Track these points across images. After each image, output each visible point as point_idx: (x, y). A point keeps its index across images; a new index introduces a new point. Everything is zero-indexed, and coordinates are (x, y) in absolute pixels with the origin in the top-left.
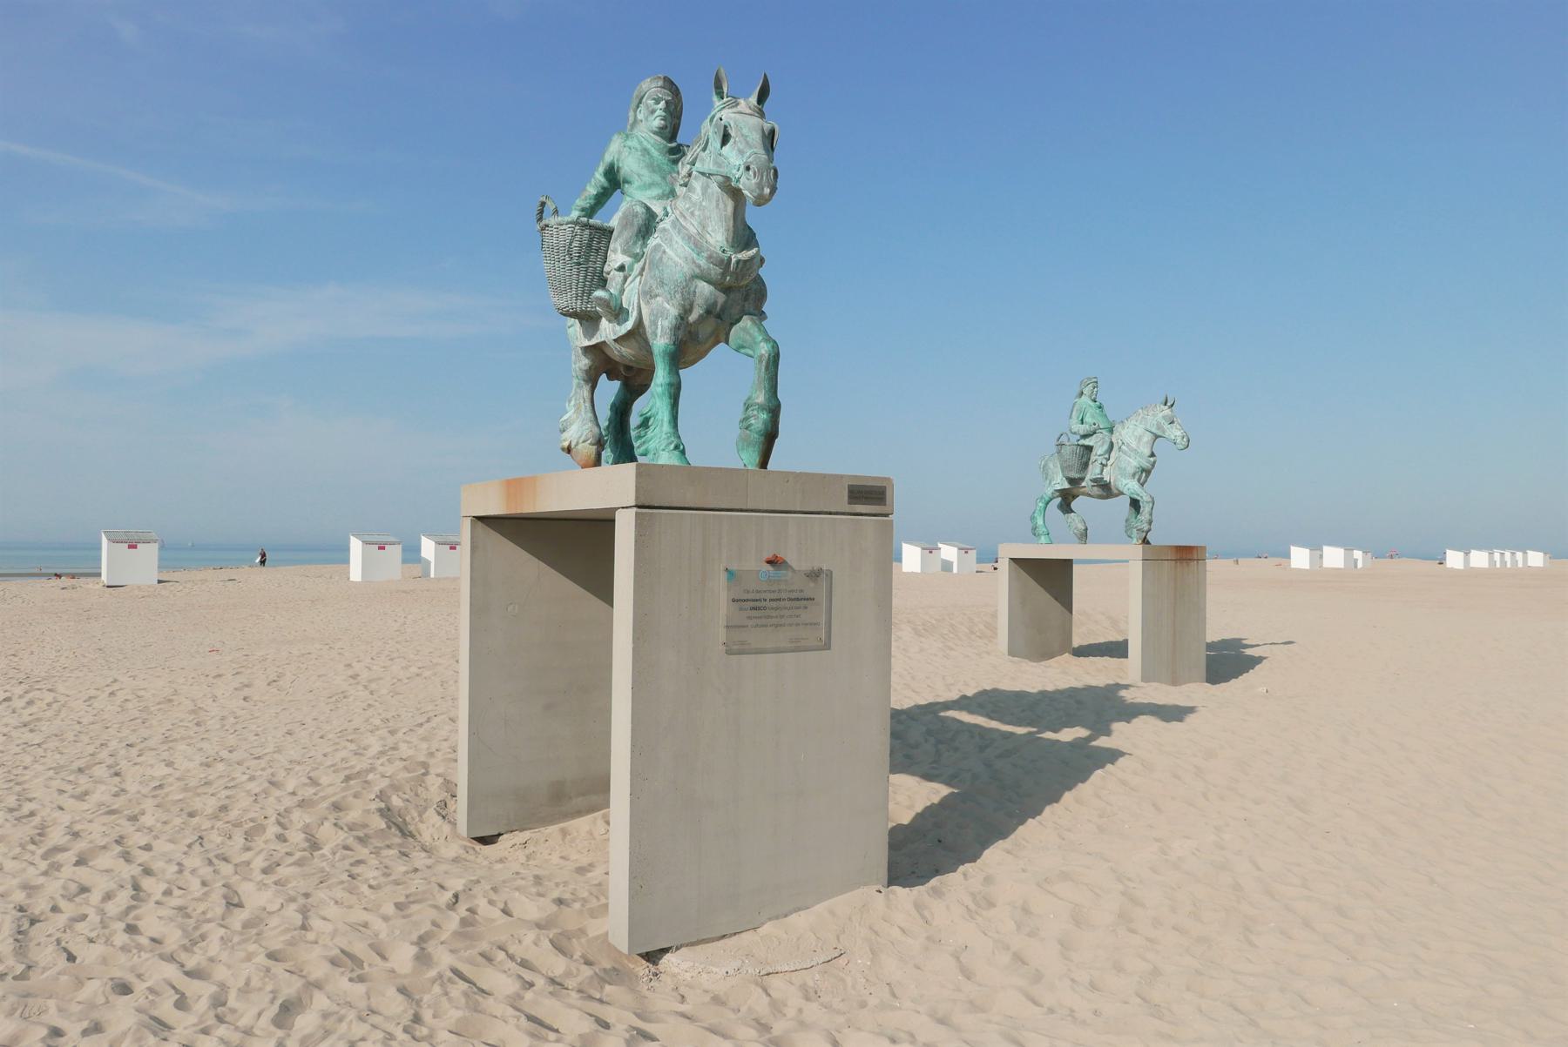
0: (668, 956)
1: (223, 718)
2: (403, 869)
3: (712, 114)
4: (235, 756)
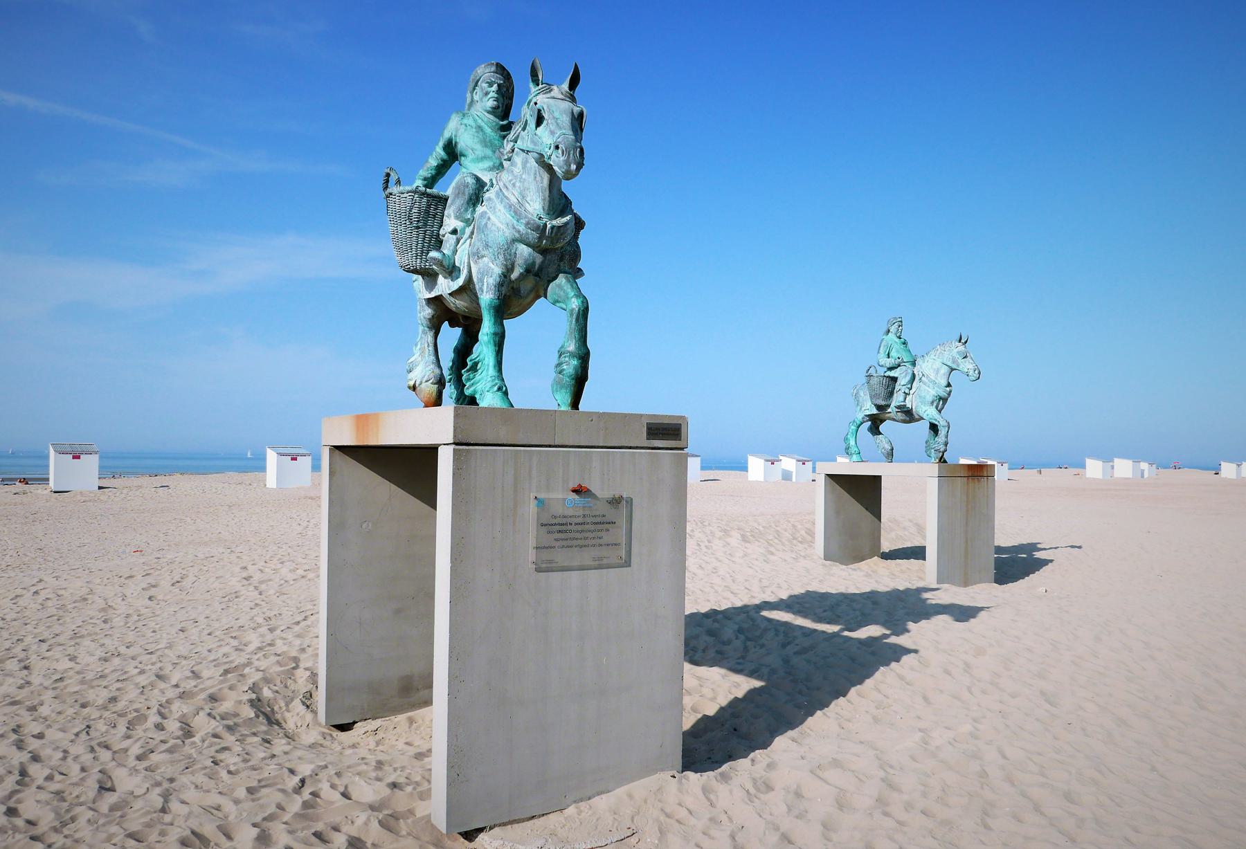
0: (481, 836)
1: (128, 616)
2: (262, 755)
3: (530, 98)
4: (132, 652)
